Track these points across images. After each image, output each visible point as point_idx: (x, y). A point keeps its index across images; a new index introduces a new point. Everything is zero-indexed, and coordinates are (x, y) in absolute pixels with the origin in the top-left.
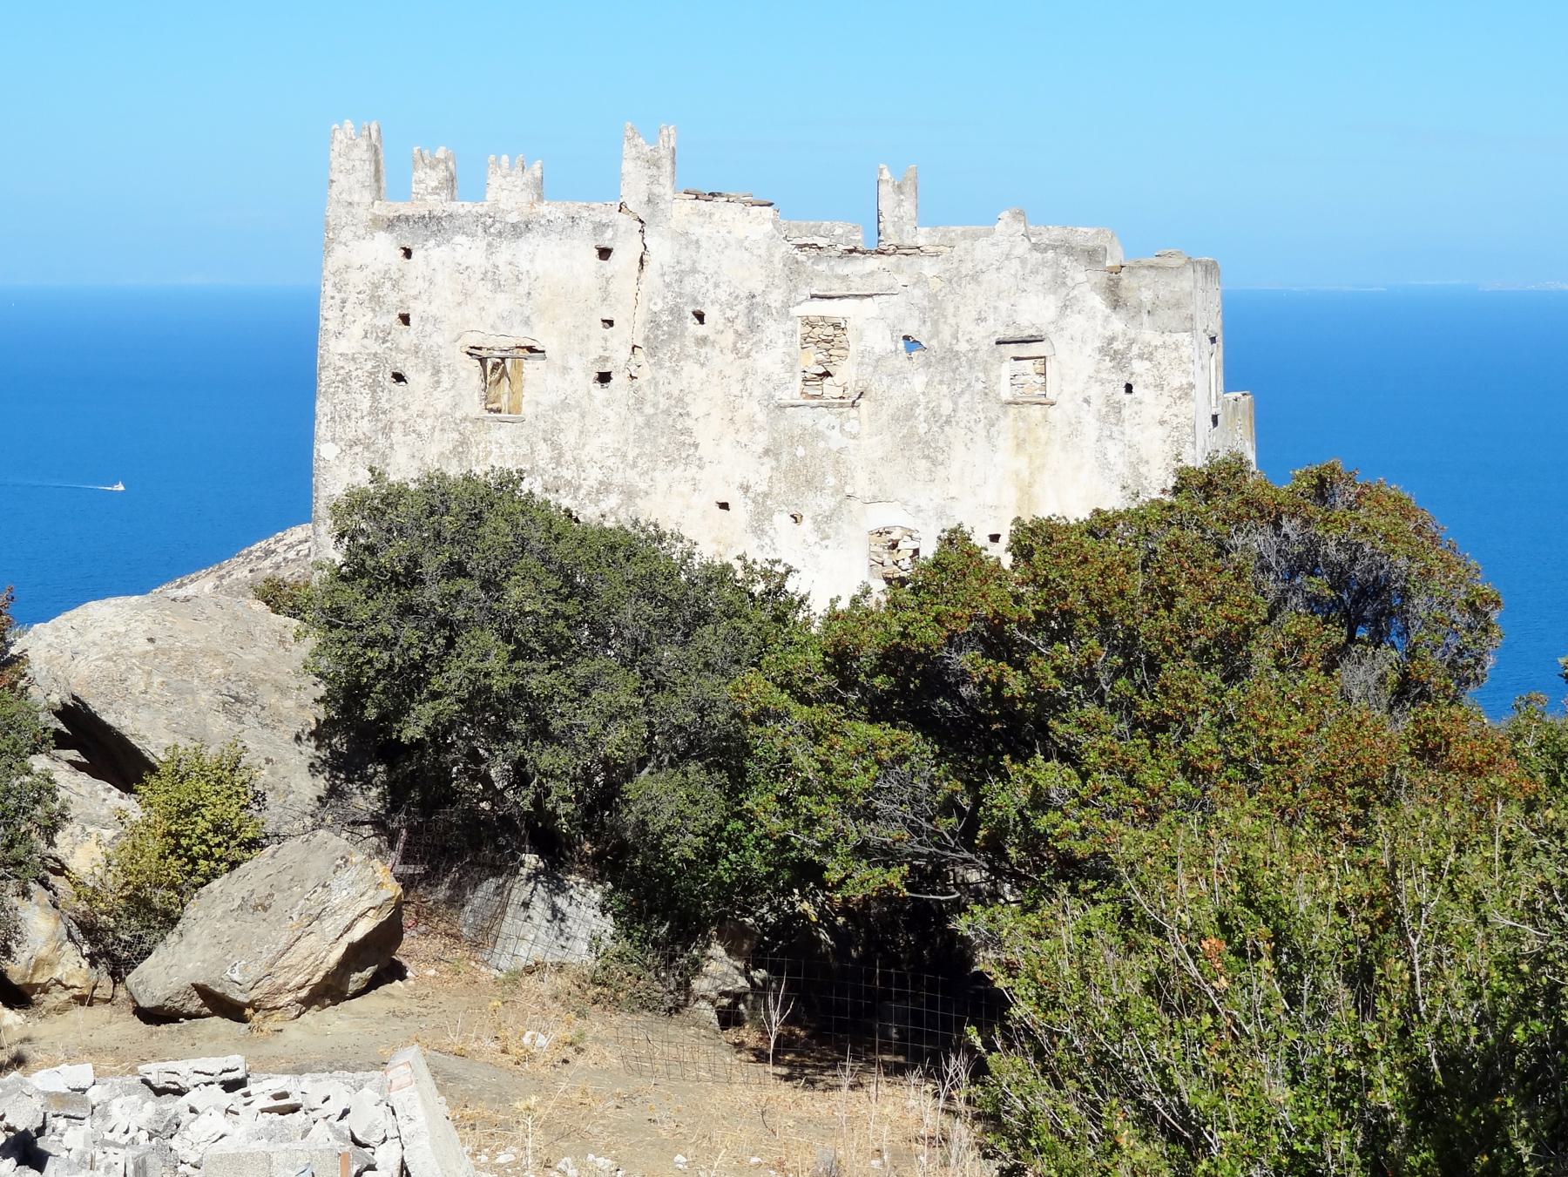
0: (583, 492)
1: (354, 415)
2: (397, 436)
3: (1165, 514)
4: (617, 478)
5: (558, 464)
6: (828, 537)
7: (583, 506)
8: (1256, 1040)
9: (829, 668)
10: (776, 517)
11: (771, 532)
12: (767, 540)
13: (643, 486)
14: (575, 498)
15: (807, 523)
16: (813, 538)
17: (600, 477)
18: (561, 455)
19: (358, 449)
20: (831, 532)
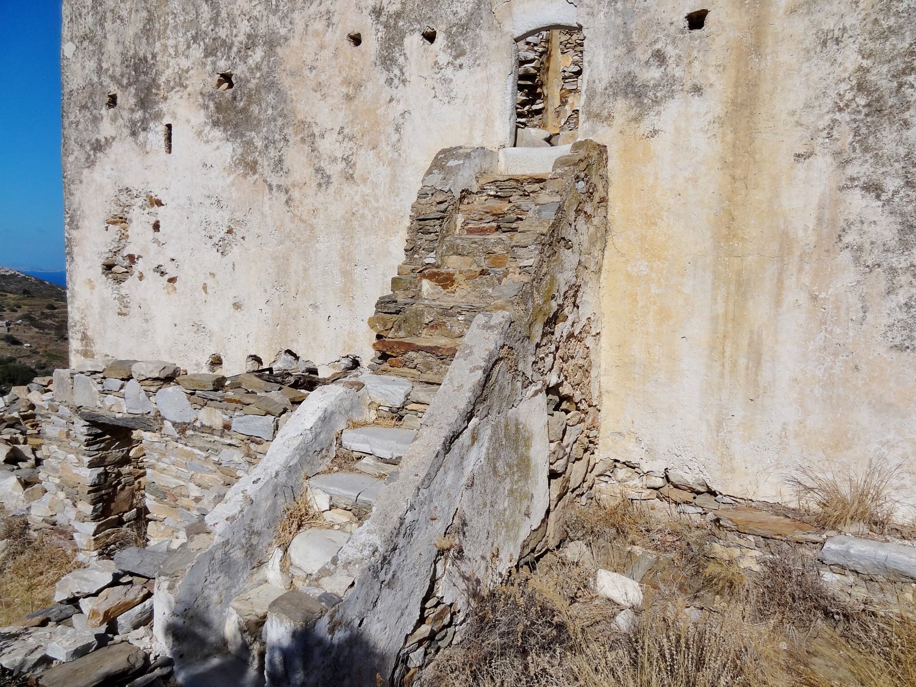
0: (235, 49)
1: (84, 11)
2: (108, 25)
3: (374, 654)
4: (262, 29)
5: (216, 24)
6: (462, 53)
7: (234, 66)
8: (838, 116)
9: (874, 41)
10: (407, 41)
11: (401, 60)
12: (397, 71)
13: (283, 31)
14: (228, 58)
15: (440, 39)
16: (444, 58)
17: (248, 30)
18: (218, 14)
19: (86, 43)
20: (467, 46)
